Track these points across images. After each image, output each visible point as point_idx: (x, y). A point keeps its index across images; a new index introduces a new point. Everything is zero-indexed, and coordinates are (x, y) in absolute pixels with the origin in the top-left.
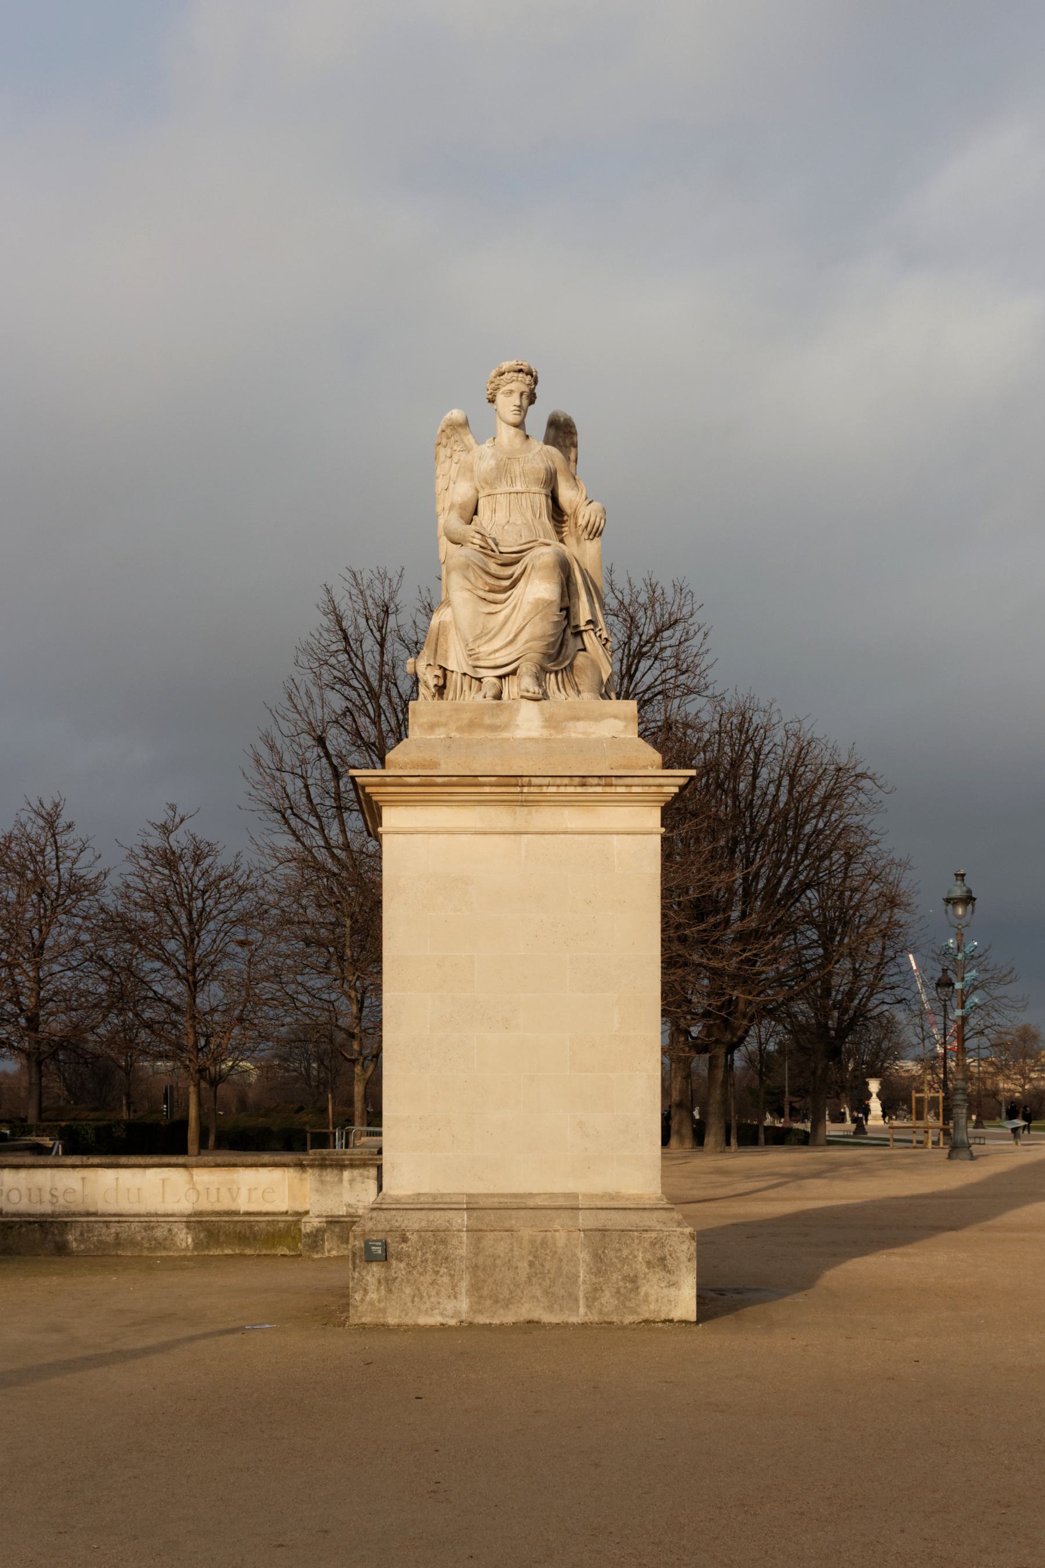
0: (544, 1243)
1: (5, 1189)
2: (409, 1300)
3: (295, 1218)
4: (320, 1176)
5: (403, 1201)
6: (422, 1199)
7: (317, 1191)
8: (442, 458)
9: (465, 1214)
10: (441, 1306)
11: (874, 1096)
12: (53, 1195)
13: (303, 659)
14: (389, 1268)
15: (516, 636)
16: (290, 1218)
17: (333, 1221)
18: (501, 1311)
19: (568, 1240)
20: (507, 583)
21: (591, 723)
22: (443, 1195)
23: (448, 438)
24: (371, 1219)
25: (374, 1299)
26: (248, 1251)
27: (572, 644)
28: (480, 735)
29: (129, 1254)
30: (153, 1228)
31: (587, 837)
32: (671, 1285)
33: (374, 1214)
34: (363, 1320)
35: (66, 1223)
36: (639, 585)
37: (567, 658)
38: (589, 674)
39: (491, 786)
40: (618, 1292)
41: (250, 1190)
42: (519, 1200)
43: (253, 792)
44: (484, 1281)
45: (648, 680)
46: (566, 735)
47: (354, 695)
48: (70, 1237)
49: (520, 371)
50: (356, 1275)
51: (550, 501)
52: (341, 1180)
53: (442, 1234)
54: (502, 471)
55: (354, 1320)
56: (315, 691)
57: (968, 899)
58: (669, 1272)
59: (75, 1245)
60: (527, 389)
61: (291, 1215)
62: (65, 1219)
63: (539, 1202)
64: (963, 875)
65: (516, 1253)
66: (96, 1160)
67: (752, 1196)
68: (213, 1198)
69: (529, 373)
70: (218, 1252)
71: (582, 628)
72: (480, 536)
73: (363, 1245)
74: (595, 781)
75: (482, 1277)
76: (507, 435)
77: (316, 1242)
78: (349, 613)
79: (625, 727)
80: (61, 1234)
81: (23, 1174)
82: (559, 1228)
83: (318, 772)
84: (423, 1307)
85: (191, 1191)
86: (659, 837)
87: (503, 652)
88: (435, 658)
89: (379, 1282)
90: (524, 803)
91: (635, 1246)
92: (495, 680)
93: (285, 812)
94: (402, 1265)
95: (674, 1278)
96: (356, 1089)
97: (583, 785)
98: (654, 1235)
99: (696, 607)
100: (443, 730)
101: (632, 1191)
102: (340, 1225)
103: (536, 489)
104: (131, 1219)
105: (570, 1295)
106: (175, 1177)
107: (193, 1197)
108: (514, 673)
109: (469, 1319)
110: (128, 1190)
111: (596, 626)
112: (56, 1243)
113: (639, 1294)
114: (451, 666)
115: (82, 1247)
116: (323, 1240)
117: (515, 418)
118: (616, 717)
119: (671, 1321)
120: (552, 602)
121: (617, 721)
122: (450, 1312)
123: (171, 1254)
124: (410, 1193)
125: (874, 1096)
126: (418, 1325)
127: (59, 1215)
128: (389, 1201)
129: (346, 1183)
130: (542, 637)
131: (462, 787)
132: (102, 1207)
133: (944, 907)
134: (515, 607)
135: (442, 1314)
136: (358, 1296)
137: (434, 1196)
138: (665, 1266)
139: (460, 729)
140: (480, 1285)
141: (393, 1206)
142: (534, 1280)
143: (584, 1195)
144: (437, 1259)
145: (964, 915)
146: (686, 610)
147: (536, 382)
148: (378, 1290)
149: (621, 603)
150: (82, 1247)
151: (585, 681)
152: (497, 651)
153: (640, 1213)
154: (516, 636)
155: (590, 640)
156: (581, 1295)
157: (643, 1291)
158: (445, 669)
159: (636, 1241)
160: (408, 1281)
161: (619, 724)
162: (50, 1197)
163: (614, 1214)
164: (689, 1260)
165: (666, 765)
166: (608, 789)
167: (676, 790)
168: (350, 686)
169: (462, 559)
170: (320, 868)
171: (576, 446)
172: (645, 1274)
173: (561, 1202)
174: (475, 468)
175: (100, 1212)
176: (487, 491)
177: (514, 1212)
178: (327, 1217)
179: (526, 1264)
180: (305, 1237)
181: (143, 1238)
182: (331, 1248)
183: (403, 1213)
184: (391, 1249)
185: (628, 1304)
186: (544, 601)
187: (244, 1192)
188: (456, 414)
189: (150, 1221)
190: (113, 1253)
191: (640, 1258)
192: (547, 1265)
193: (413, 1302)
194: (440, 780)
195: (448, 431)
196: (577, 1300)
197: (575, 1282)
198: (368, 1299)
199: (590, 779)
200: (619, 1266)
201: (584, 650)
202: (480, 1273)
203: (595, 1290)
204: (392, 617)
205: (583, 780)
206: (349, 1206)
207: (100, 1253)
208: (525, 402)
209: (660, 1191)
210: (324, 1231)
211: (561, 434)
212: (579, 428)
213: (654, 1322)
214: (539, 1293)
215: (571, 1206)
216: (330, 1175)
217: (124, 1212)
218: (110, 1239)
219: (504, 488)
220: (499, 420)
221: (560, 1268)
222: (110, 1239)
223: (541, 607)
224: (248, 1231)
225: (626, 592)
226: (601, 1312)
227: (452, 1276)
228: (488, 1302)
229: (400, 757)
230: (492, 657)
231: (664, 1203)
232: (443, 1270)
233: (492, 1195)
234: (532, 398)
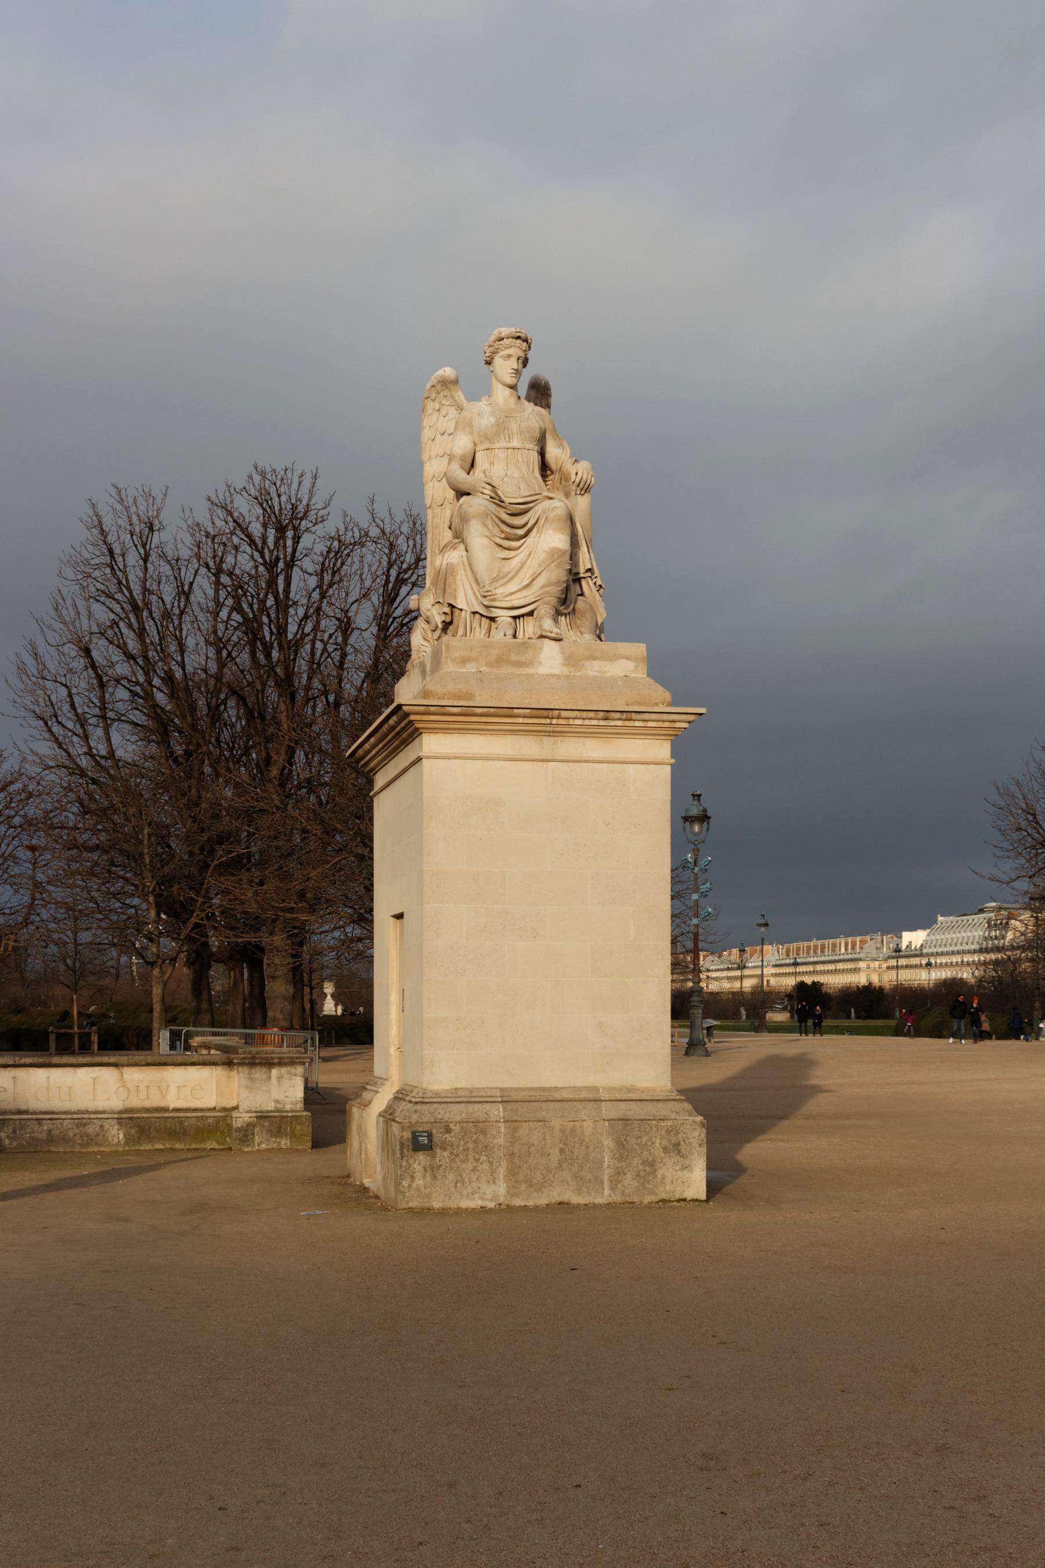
0: (573, 1131)
2: (452, 1185)
3: (223, 1114)
4: (249, 1074)
5: (443, 1095)
6: (460, 1093)
7: (247, 1088)
8: (429, 411)
10: (482, 1191)
11: (329, 997)
13: (69, 573)
14: (434, 1156)
16: (219, 1114)
17: (262, 1116)
18: (535, 1194)
20: (522, 532)
21: (606, 663)
22: (478, 1089)
23: (438, 393)
24: (416, 1112)
26: (178, 1146)
28: (506, 670)
30: (85, 1124)
31: (605, 765)
32: (685, 1168)
34: (411, 1205)
36: (400, 516)
39: (524, 717)
40: (638, 1175)
41: (178, 1087)
42: (547, 1094)
43: (17, 699)
44: (520, 1167)
47: (117, 608)
49: (519, 338)
52: (269, 1078)
53: (482, 1125)
54: (501, 428)
56: (81, 605)
57: (704, 818)
58: (682, 1156)
59: (7, 1142)
60: (523, 355)
61: (219, 1111)
63: (565, 1095)
64: (699, 796)
65: (549, 1142)
66: (28, 1060)
68: (143, 1095)
69: (526, 340)
70: (149, 1147)
73: (410, 1136)
74: (618, 715)
76: (502, 395)
77: (246, 1136)
78: (114, 529)
82: (585, 1118)
83: (83, 682)
84: (465, 1192)
85: (121, 1089)
86: (669, 767)
89: (425, 1170)
90: (551, 734)
92: (511, 620)
93: (48, 720)
94: (446, 1154)
95: (687, 1162)
96: (155, 991)
98: (669, 1123)
100: (473, 664)
101: (645, 1085)
103: (531, 446)
104: (64, 1116)
105: (596, 1178)
106: (106, 1076)
108: (531, 614)
111: (593, 574)
114: (460, 604)
115: (15, 1144)
116: (253, 1134)
118: (627, 658)
119: (685, 1200)
122: (489, 1196)
124: (448, 1087)
125: (329, 997)
129: (274, 1081)
131: (468, 717)
132: (33, 1105)
133: (682, 824)
135: (482, 1198)
137: (471, 1091)
138: (679, 1151)
139: (489, 664)
140: (516, 1171)
141: (435, 1100)
142: (564, 1165)
143: (604, 1088)
144: (477, 1147)
145: (701, 831)
148: (424, 1177)
149: (383, 532)
150: (15, 1144)
152: (513, 593)
153: (655, 1103)
156: (606, 1178)
157: (660, 1173)
158: (452, 607)
159: (654, 1129)
160: (451, 1168)
161: (631, 665)
163: (632, 1106)
164: (700, 1145)
166: (627, 723)
168: (115, 599)
169: (482, 508)
170: (83, 774)
173: (584, 1095)
174: (475, 423)
175: (31, 1109)
178: (256, 1112)
179: (557, 1152)
180: (236, 1131)
181: (75, 1135)
182: (261, 1141)
185: (647, 1186)
186: (558, 549)
187: (173, 1090)
188: (448, 372)
189: (82, 1118)
190: (45, 1149)
192: (576, 1151)
193: (456, 1187)
195: (439, 387)
196: (602, 1183)
197: (601, 1167)
198: (414, 1185)
200: (639, 1151)
201: (582, 595)
202: (516, 1160)
203: (618, 1173)
204: (156, 534)
205: (607, 714)
206: (277, 1101)
208: (521, 366)
210: (254, 1126)
212: (554, 391)
213: (670, 1201)
214: (569, 1178)
215: (593, 1099)
216: (258, 1073)
217: (55, 1109)
218: (43, 1136)
219: (503, 444)
220: (494, 381)
221: (587, 1154)
222: (43, 1136)
223: (556, 556)
224: (178, 1126)
225: (387, 521)
226: (623, 1193)
227: (491, 1163)
228: (524, 1186)
230: (508, 598)
231: (674, 1095)
232: (483, 1158)
234: (525, 362)
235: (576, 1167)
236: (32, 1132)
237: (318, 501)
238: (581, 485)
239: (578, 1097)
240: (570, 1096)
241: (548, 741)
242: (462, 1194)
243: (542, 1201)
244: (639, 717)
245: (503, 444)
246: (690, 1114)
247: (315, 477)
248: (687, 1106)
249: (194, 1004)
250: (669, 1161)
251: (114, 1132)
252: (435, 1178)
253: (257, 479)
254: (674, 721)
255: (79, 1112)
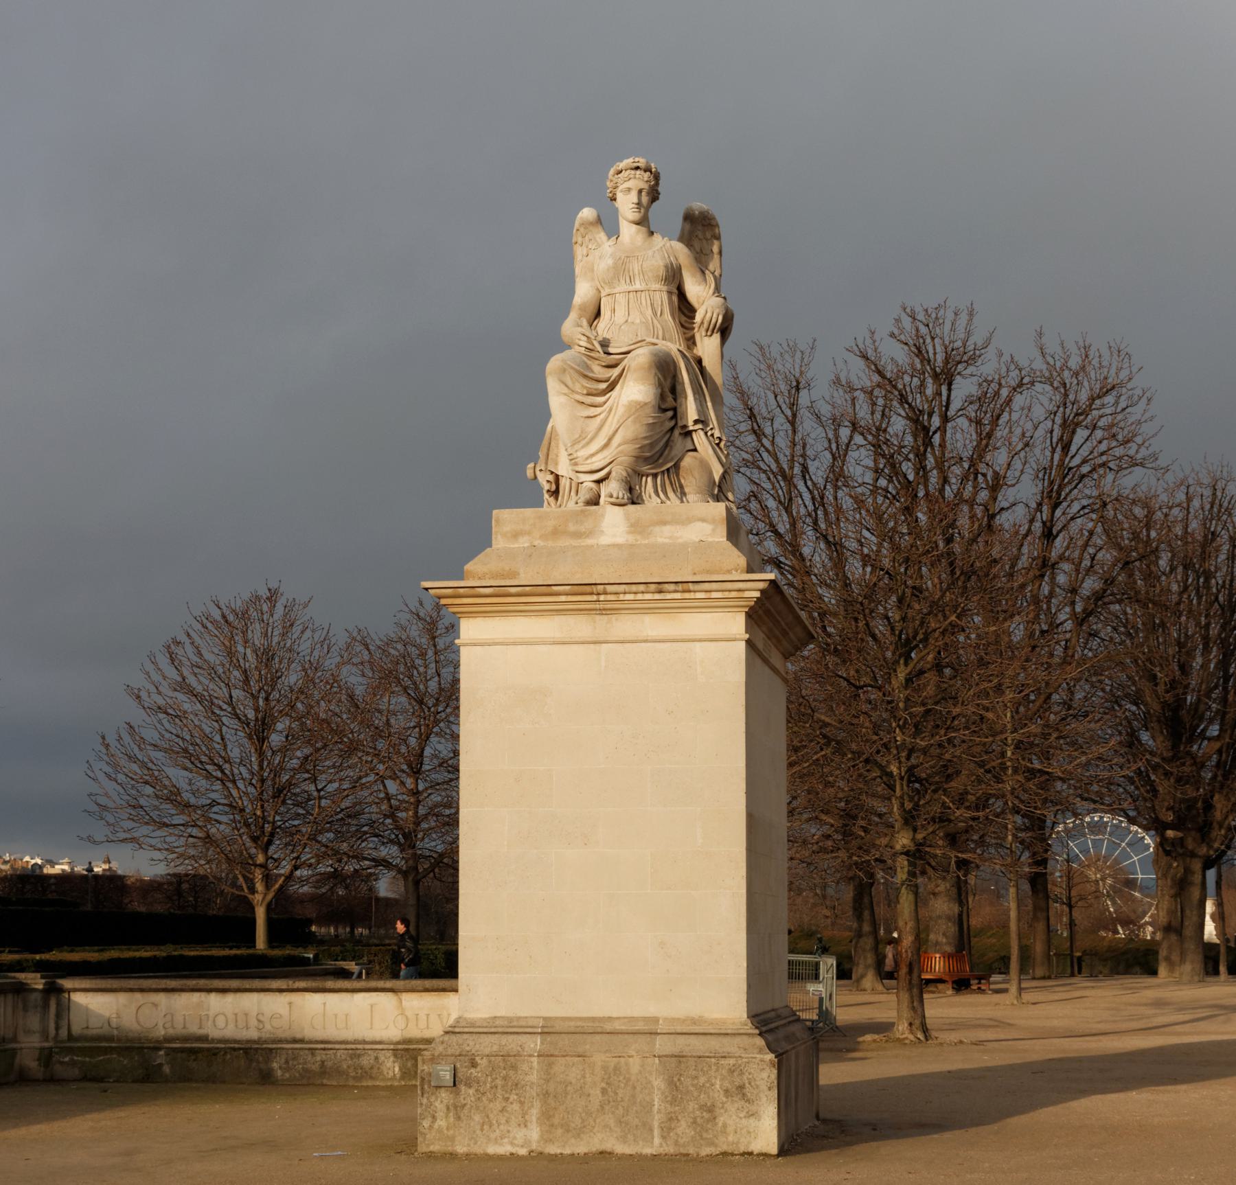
0: (617, 1069)
1: (211, 1013)
2: (478, 1127)
12: (259, 1021)
14: (458, 1094)
15: (610, 440)
18: (573, 1141)
19: (642, 1066)
20: (604, 386)
22: (519, 1018)
25: (443, 1128)
27: (679, 443)
29: (335, 1083)
30: (359, 1056)
31: (668, 644)
32: (751, 1115)
33: (446, 1038)
34: (432, 1148)
35: (271, 1050)
37: (672, 460)
38: (697, 475)
39: (567, 594)
40: (695, 1122)
45: (1084, 452)
48: (275, 1065)
49: (637, 168)
51: (675, 298)
54: (620, 270)
55: (422, 1148)
58: (748, 1101)
59: (279, 1073)
60: (646, 186)
62: (270, 1046)
63: (618, 1026)
65: (589, 1080)
67: (1166, 1029)
68: (422, 1024)
71: (691, 428)
72: (585, 338)
74: (672, 587)
75: (553, 1104)
79: (713, 530)
81: (230, 998)
88: (546, 463)
89: (448, 1109)
90: (602, 612)
92: (593, 485)
94: (471, 1091)
95: (753, 1108)
97: (660, 592)
98: (732, 1061)
100: (526, 538)
101: (716, 1015)
103: (657, 286)
104: (337, 1046)
105: (644, 1124)
106: (384, 1001)
107: (401, 1023)
109: (540, 1149)
110: (336, 1016)
113: (716, 1124)
115: (287, 1075)
117: (636, 216)
118: (703, 520)
119: (751, 1154)
120: (646, 404)
122: (519, 1141)
123: (378, 1083)
126: (487, 1155)
127: (266, 1042)
128: (464, 1024)
130: (634, 440)
132: (309, 1033)
134: (610, 410)
135: (512, 1144)
136: (426, 1123)
137: (510, 1019)
138: (744, 1095)
139: (543, 537)
141: (466, 1030)
142: (607, 1108)
143: (665, 1019)
146: (1124, 375)
147: (657, 177)
148: (447, 1117)
151: (691, 482)
153: (720, 1038)
155: (699, 439)
156: (656, 1124)
160: (477, 1108)
161: (707, 528)
162: (256, 1023)
163: (693, 1040)
164: (770, 1089)
165: (750, 570)
166: (687, 595)
167: (758, 594)
168: (760, 468)
171: (718, 238)
173: (640, 1026)
176: (607, 291)
177: (589, 1037)
184: (459, 1075)
185: (705, 1135)
186: (638, 403)
189: (356, 1048)
190: (319, 1082)
192: (621, 1092)
193: (482, 1130)
194: (513, 590)
195: (582, 230)
196: (651, 1130)
197: (650, 1111)
198: (436, 1126)
200: (696, 1094)
201: (695, 450)
203: (671, 1119)
205: (660, 586)
207: (305, 1082)
208: (645, 199)
209: (745, 1016)
211: (700, 228)
213: (733, 1154)
214: (612, 1123)
215: (649, 1031)
218: (316, 1067)
219: (623, 287)
221: (633, 1096)
222: (316, 1067)
226: (676, 1143)
227: (522, 1103)
228: (560, 1131)
229: (480, 569)
232: (513, 1097)
234: (654, 195)
235: (620, 1111)
236: (305, 1063)
237: (977, 339)
238: (706, 325)
241: (601, 620)
242: (489, 1139)
243: (581, 1148)
246: (761, 1051)
247: (971, 314)
248: (760, 1042)
251: (389, 1064)
253: (907, 322)
254: (739, 590)
255: (356, 1042)
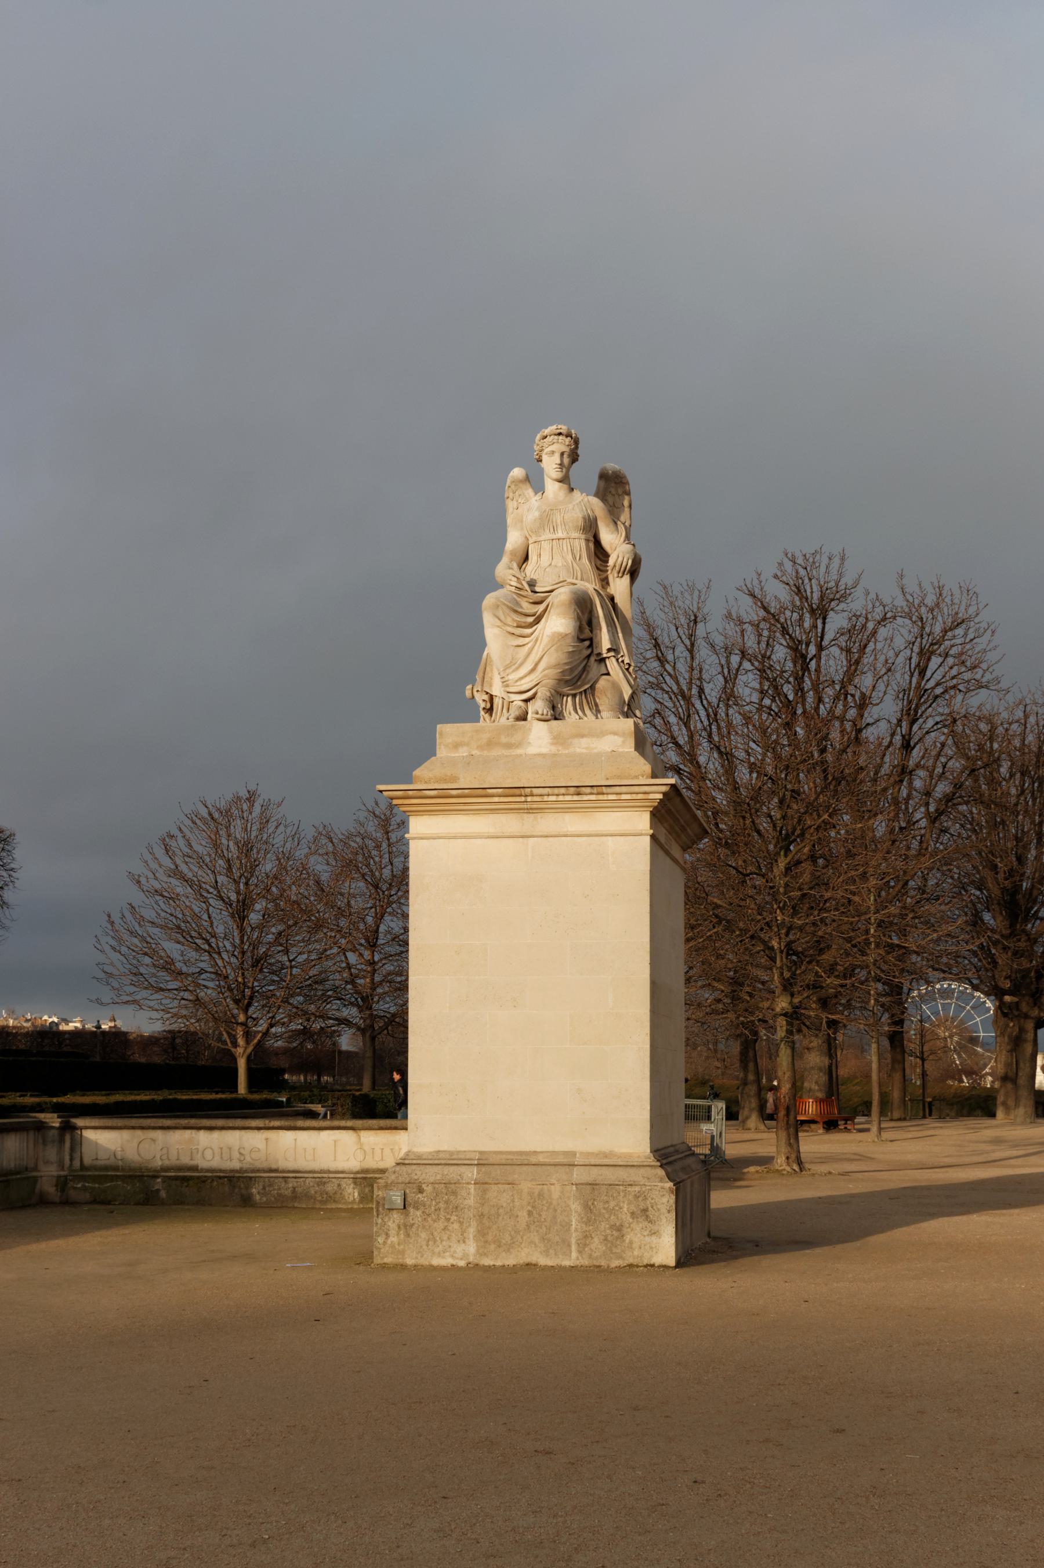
0: (541, 1195)
2: (424, 1243)
6: (441, 1156)
9: (475, 1168)
12: (240, 1154)
14: (407, 1215)
15: (536, 665)
18: (504, 1254)
19: (562, 1192)
20: (531, 619)
22: (459, 1152)
23: (514, 493)
25: (397, 1244)
27: (595, 668)
30: (325, 1183)
32: (653, 1233)
33: (398, 1168)
34: (386, 1260)
35: (251, 1178)
38: (609, 695)
39: (500, 796)
40: (606, 1239)
44: (489, 1228)
45: (938, 676)
46: (571, 750)
48: (254, 1191)
49: (560, 434)
50: (380, 1221)
53: (453, 1186)
54: (545, 521)
55: (378, 1260)
58: (650, 1222)
59: (258, 1197)
60: (567, 449)
63: (541, 1159)
65: (517, 1204)
66: (277, 1123)
68: (378, 1157)
71: (605, 655)
74: (588, 790)
79: (624, 742)
80: (247, 1188)
81: (216, 1134)
87: (527, 679)
88: (482, 685)
89: (399, 1227)
90: (529, 811)
91: (621, 1198)
92: (522, 704)
94: (419, 1213)
95: (655, 1228)
97: (579, 794)
99: (981, 606)
100: (465, 748)
101: (624, 1150)
102: (367, 1179)
103: (576, 535)
104: (306, 1175)
105: (564, 1241)
109: (476, 1261)
112: (242, 1196)
117: (559, 475)
118: (615, 734)
119: (652, 1266)
120: (566, 635)
121: (616, 737)
122: (459, 1255)
124: (432, 1150)
126: (432, 1266)
127: (246, 1171)
128: (412, 1157)
130: (555, 666)
131: (451, 798)
132: (282, 1164)
134: (537, 640)
135: (452, 1256)
136: (381, 1240)
137: (451, 1153)
139: (480, 747)
141: (415, 1162)
142: (532, 1227)
143: (581, 1153)
146: (972, 610)
147: (576, 442)
151: (605, 701)
154: (536, 665)
155: (612, 665)
156: (573, 1241)
157: (627, 1238)
160: (424, 1227)
161: (618, 740)
164: (669, 1212)
165: (654, 776)
166: (601, 797)
167: (661, 796)
171: (628, 494)
172: (630, 1224)
177: (517, 1168)
179: (525, 1214)
183: (422, 1167)
184: (409, 1199)
185: (614, 1250)
186: (560, 634)
189: (322, 1177)
190: (291, 1205)
191: (625, 1209)
192: (544, 1214)
194: (454, 792)
195: (513, 486)
196: (569, 1246)
197: (569, 1230)
198: (389, 1242)
199: (583, 789)
200: (607, 1216)
201: (608, 674)
202: (485, 1221)
203: (586, 1237)
205: (578, 789)
208: (566, 461)
212: (630, 478)
213: (638, 1266)
214: (536, 1240)
215: (567, 1163)
218: (288, 1193)
221: (555, 1218)
222: (288, 1193)
226: (590, 1256)
227: (461, 1223)
228: (493, 1246)
233: (501, 1153)
234: (574, 457)
237: (848, 580)
238: (617, 568)
239: (552, 1161)
240: (547, 1160)
243: (510, 1260)
244: (609, 790)
245: (549, 536)
246: (661, 1180)
247: (843, 559)
248: (661, 1172)
249: (742, 1075)
250: (637, 1227)
252: (408, 1235)
253: (788, 566)
255: (322, 1172)
